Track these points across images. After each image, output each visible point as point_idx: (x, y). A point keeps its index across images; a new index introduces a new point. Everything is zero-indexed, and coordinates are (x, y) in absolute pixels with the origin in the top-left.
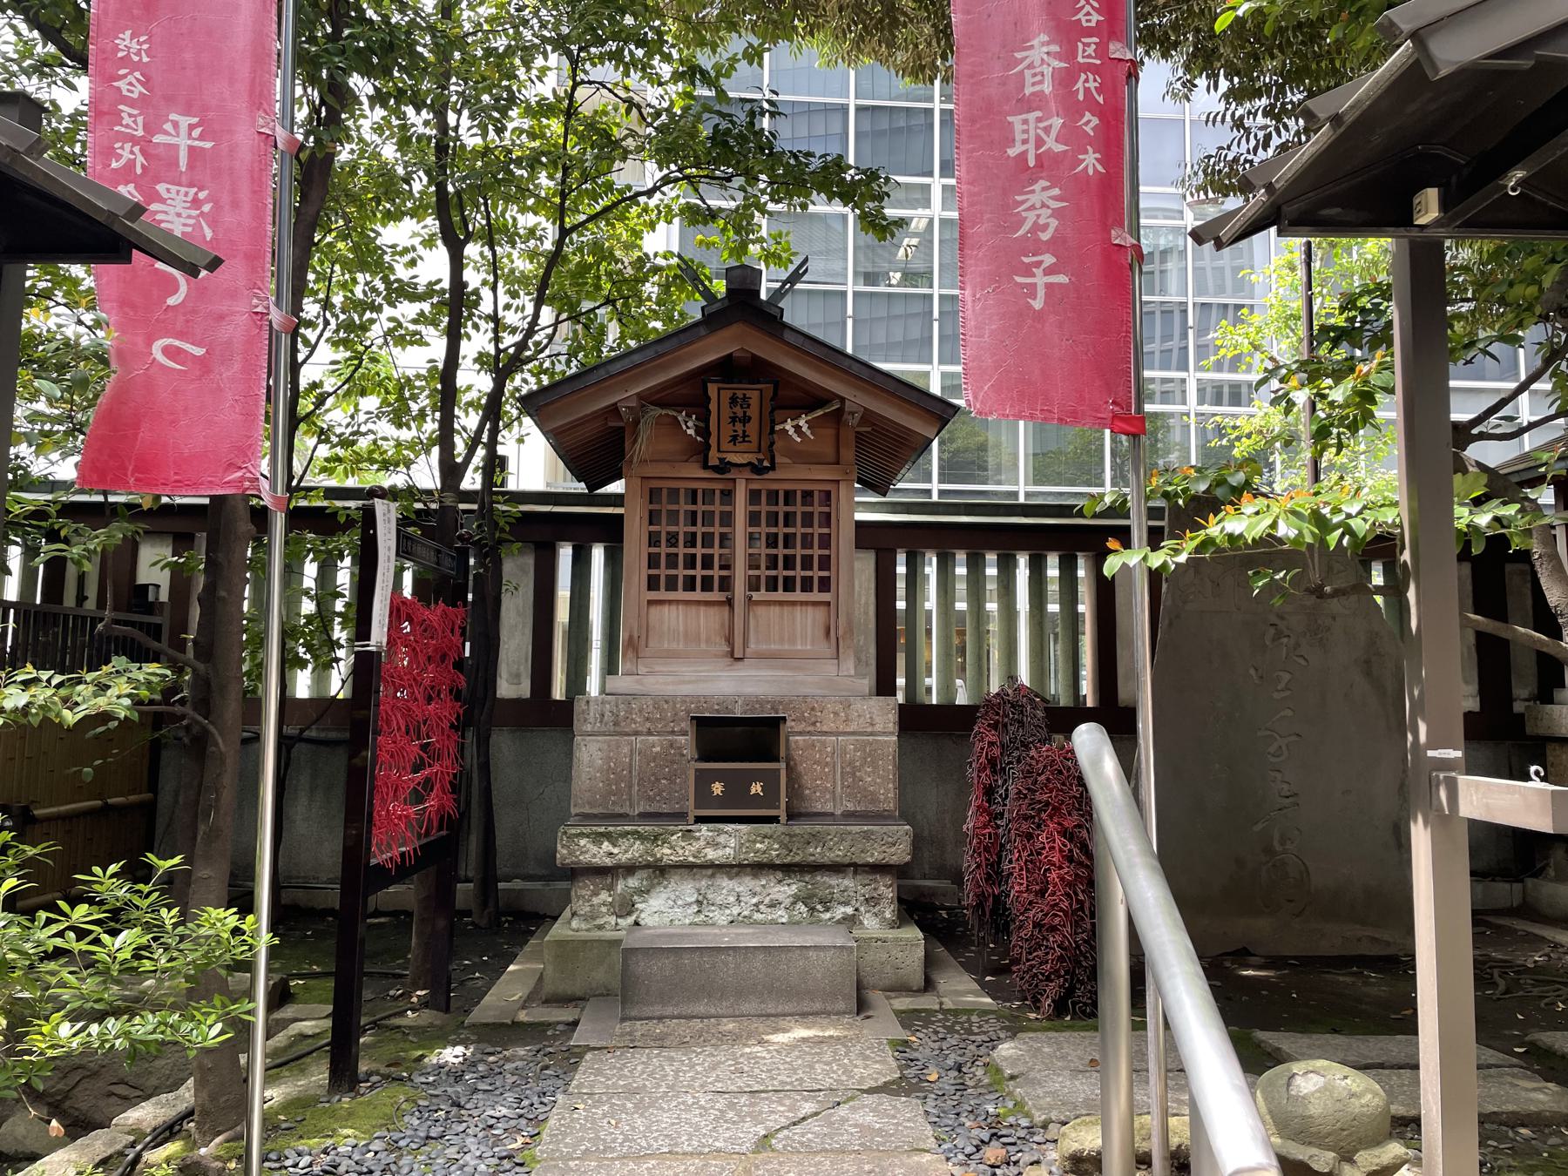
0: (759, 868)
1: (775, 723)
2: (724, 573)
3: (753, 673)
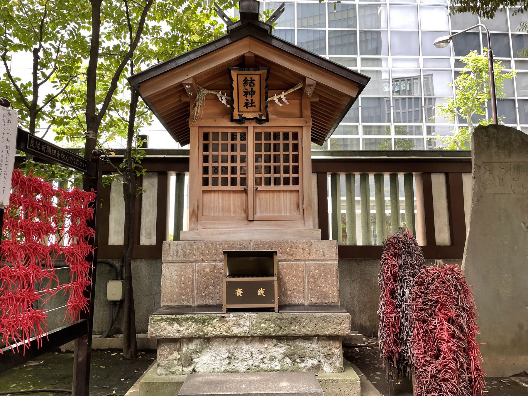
0: (263, 338)
1: (271, 255)
2: (243, 176)
3: (181, 70)
